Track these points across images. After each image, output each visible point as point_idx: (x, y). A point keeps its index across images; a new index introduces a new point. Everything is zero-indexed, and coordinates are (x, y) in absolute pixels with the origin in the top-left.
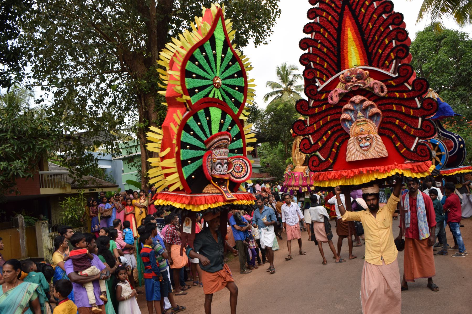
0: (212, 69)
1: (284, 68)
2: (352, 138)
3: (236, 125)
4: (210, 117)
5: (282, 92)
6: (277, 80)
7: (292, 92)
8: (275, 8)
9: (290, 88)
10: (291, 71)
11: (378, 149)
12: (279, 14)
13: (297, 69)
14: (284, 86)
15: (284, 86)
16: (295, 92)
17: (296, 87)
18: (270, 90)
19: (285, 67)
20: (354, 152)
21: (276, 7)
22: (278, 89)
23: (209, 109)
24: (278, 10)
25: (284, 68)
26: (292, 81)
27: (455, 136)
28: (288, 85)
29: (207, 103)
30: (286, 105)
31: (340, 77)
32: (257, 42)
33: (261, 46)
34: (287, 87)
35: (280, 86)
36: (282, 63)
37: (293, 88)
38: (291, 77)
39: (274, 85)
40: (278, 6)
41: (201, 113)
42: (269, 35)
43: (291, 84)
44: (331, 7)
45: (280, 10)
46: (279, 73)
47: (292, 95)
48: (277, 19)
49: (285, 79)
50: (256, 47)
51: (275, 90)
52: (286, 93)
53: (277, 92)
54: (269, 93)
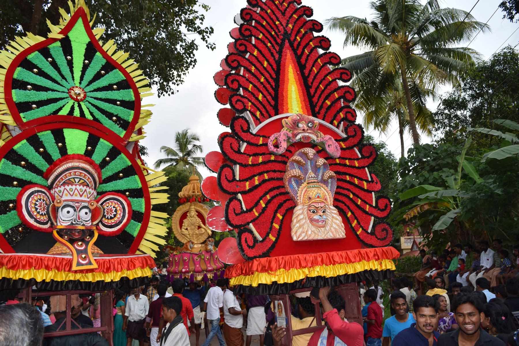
0: (93, 105)
1: (185, 135)
2: (299, 207)
3: (101, 140)
4: (64, 143)
5: (177, 161)
6: (174, 146)
7: (188, 163)
8: (190, 57)
9: (187, 158)
10: (192, 140)
11: (334, 228)
12: (193, 64)
13: (198, 139)
14: (181, 155)
15: (181, 155)
16: (191, 164)
17: (194, 158)
18: (163, 156)
19: (186, 134)
20: (302, 229)
21: (192, 55)
22: (173, 157)
23: (62, 133)
24: (193, 60)
25: (185, 135)
26: (190, 151)
27: (76, 249)
28: (185, 155)
29: (58, 125)
30: (180, 174)
31: (283, 120)
32: (163, 89)
33: (165, 97)
34: (184, 156)
35: (176, 154)
36: (183, 129)
37: (190, 160)
38: (190, 147)
39: (169, 151)
40: (194, 55)
41: (46, 137)
42: (178, 85)
43: (189, 154)
44: (267, 46)
45: (195, 61)
46: (177, 139)
47: (187, 166)
48: (190, 69)
49: (184, 148)
50: (159, 97)
51: (170, 157)
52: (181, 163)
53: (172, 160)
54: (163, 160)
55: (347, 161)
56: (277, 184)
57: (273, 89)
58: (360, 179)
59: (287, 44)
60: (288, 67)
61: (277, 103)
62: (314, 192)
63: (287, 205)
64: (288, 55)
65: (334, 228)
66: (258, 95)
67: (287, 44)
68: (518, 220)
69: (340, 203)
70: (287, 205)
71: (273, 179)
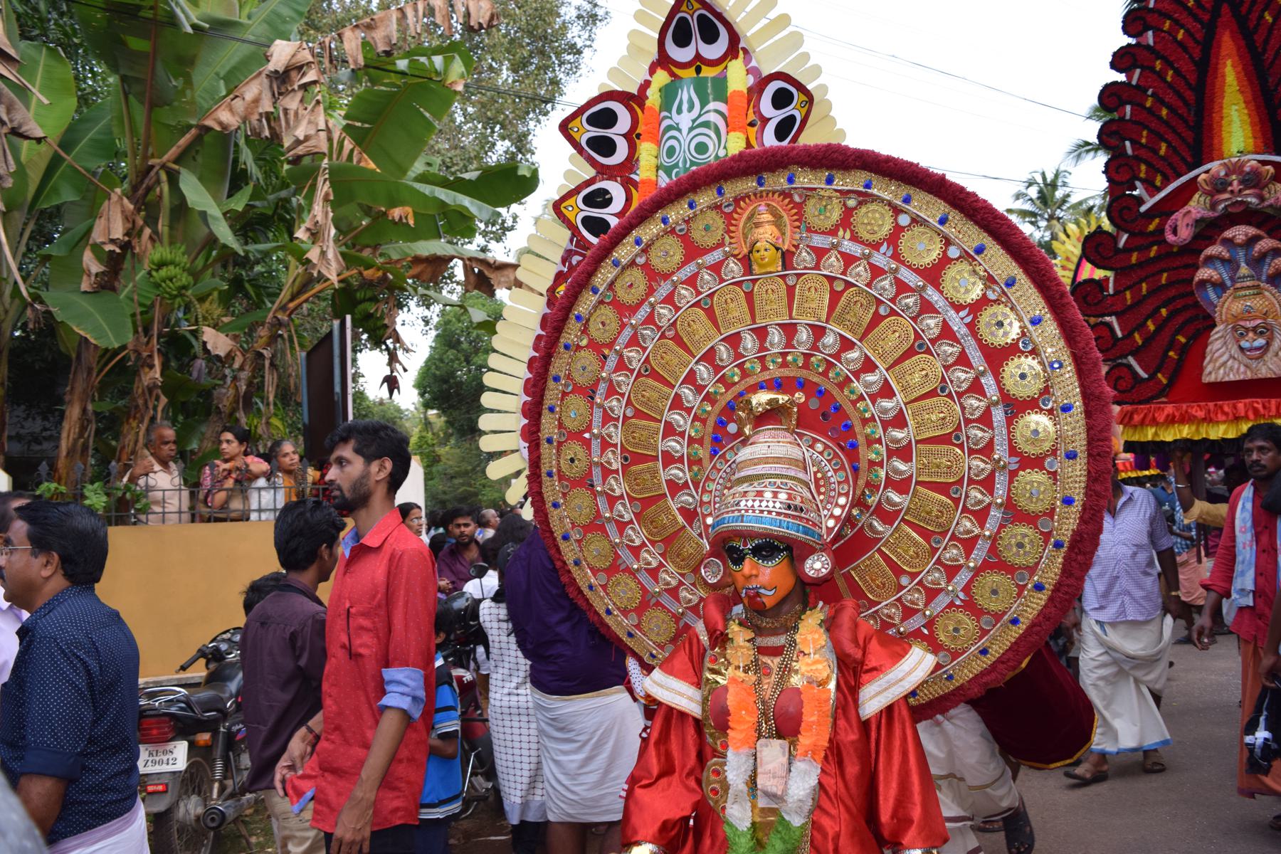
2: (1220, 327)
60: (1225, 66)
61: (1201, 143)
64: (1227, 43)
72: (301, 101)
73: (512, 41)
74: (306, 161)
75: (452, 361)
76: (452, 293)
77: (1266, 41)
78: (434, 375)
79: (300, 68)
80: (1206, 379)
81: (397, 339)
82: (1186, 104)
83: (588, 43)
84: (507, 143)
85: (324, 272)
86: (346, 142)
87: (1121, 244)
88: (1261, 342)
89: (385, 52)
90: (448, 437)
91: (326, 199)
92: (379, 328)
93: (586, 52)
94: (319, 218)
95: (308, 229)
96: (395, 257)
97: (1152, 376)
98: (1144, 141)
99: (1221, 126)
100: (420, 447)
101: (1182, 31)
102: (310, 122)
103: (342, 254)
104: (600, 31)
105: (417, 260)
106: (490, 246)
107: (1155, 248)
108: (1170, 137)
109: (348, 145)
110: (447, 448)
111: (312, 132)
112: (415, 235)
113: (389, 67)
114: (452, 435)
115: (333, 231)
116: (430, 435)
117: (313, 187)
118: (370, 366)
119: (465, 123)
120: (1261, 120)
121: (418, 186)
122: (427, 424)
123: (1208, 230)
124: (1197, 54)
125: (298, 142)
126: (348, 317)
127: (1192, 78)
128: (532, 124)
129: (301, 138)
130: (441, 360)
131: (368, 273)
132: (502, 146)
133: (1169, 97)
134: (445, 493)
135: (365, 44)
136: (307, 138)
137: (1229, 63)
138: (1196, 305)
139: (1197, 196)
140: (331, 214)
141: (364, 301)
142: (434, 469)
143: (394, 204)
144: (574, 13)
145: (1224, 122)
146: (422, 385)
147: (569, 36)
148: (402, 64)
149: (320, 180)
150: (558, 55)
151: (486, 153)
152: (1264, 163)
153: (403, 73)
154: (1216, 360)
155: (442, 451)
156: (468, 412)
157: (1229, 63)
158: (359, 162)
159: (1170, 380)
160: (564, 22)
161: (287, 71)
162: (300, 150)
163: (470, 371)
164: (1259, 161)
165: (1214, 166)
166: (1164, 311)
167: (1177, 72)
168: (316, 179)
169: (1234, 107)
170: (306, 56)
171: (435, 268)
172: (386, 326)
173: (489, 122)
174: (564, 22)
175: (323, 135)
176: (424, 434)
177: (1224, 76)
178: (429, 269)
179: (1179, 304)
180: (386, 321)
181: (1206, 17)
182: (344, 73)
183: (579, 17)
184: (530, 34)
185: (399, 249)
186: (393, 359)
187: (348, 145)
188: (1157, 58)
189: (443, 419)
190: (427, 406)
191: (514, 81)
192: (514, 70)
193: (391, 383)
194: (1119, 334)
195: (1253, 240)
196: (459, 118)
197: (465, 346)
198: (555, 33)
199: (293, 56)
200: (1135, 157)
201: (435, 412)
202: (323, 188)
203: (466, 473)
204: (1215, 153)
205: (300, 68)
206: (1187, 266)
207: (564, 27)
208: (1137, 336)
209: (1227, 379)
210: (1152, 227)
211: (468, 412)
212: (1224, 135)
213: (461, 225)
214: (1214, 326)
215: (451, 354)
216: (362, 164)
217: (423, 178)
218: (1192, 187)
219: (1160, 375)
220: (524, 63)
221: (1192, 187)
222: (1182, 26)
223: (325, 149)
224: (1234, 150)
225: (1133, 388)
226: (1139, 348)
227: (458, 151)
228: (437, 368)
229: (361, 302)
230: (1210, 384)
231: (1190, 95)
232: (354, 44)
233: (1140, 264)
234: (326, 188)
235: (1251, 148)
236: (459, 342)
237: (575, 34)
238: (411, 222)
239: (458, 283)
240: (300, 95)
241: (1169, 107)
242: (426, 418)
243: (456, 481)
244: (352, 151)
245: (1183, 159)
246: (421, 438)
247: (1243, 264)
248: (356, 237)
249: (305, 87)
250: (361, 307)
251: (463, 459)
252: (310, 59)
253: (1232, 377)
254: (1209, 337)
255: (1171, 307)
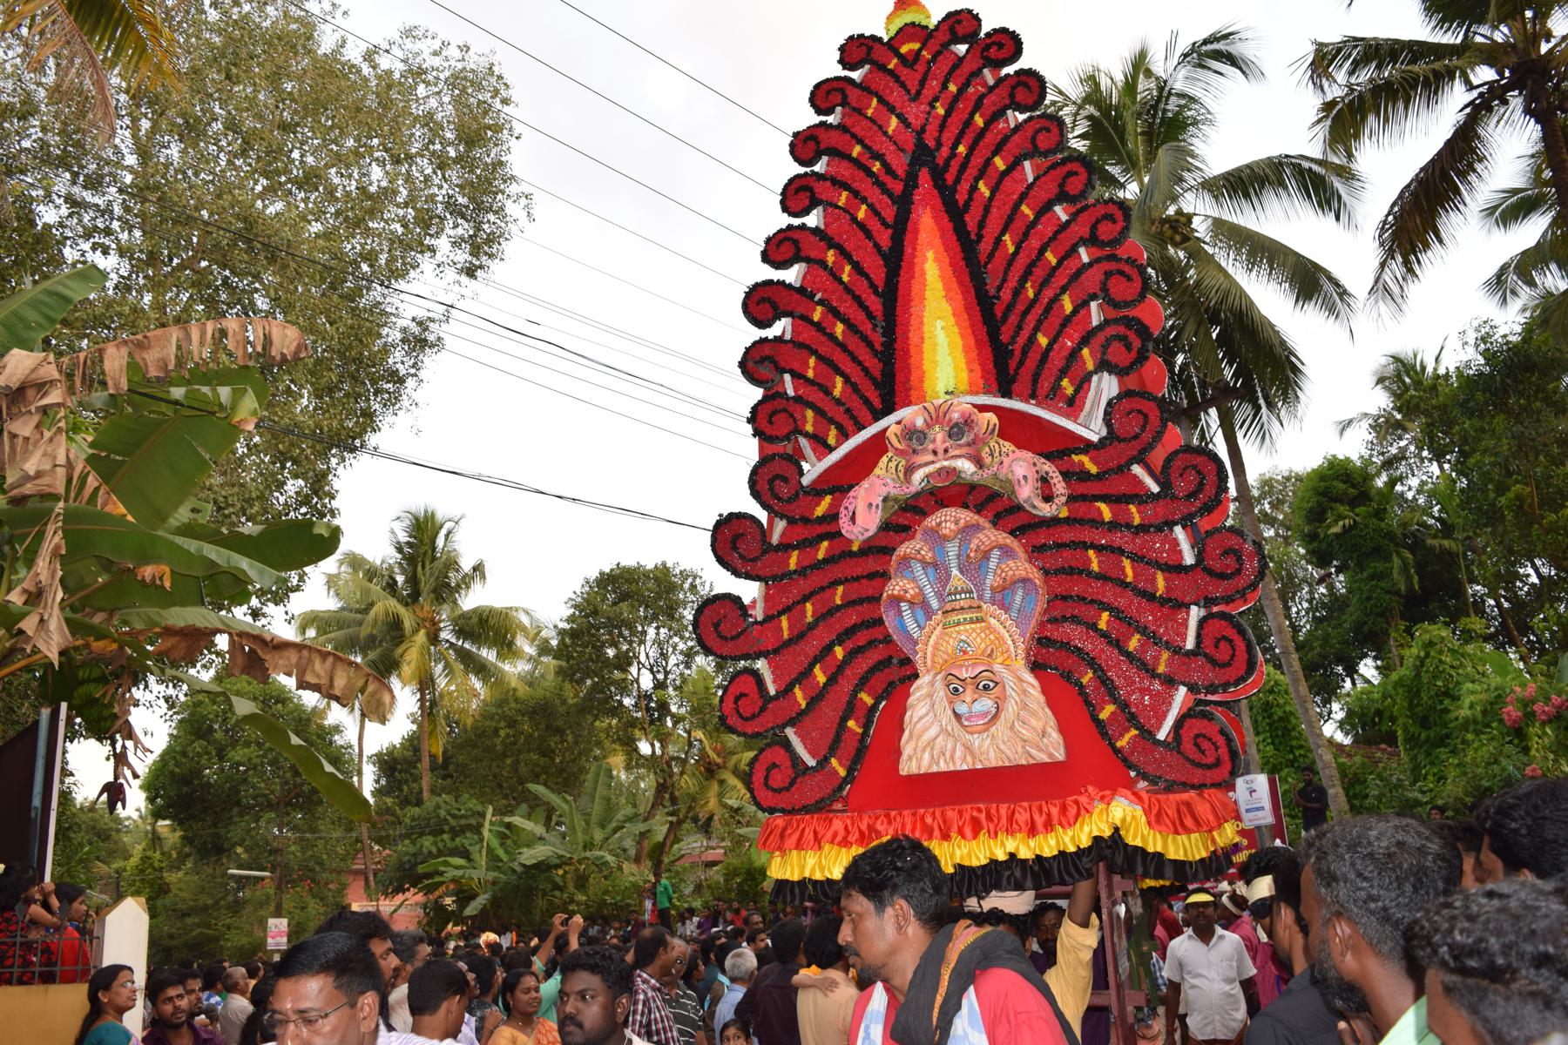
2: (924, 680)
11: (1026, 730)
55: (1104, 715)
56: (872, 657)
57: (877, 385)
58: (1115, 500)
59: (924, 176)
60: (925, 260)
61: (891, 381)
62: (969, 635)
63: (895, 673)
64: (927, 225)
65: (1026, 730)
66: (843, 392)
67: (924, 176)
68: (1530, 8)
69: (1049, 658)
70: (895, 673)
71: (859, 650)
72: (37, 427)
73: (319, 362)
74: (32, 505)
75: (199, 755)
76: (204, 674)
77: (981, 225)
78: (172, 773)
79: (42, 387)
80: (908, 767)
81: (129, 734)
82: (870, 315)
83: (413, 371)
84: (301, 482)
85: (42, 646)
86: (90, 478)
87: (775, 539)
88: (986, 704)
89: (158, 378)
90: (182, 858)
91: (55, 553)
92: (105, 719)
93: (410, 383)
94: (43, 578)
95: (25, 591)
96: (139, 626)
97: (823, 762)
98: (810, 374)
99: (921, 352)
100: (142, 871)
101: (864, 207)
102: (45, 454)
103: (68, 621)
104: (430, 360)
105: (169, 631)
106: (265, 610)
107: (825, 544)
108: (849, 367)
109: (92, 481)
110: (180, 874)
111: (48, 467)
112: (169, 599)
113: (160, 395)
114: (189, 855)
115: (60, 594)
116: (157, 855)
117: (40, 536)
118: (86, 765)
119: (248, 456)
120: (977, 341)
121: (180, 540)
122: (155, 839)
123: (906, 517)
124: (885, 238)
125: (27, 478)
126: (64, 705)
127: (879, 275)
128: (334, 461)
129: (32, 473)
130: (184, 754)
131: (98, 646)
132: (293, 486)
133: (847, 306)
134: (171, 936)
135: (133, 366)
136: (39, 475)
137: (930, 255)
138: (887, 640)
139: (885, 459)
140: (60, 573)
141: (88, 681)
142: (159, 903)
143: (146, 559)
144: (399, 335)
145: (926, 347)
146: (153, 787)
147: (391, 361)
148: (178, 393)
149: (51, 528)
150: (374, 382)
151: (271, 492)
152: (983, 408)
153: (176, 403)
154: (920, 736)
155: (172, 877)
156: (215, 825)
157: (930, 255)
158: (105, 504)
159: (850, 771)
160: (385, 344)
161: (22, 389)
162: (28, 489)
163: (222, 769)
164: (975, 406)
165: (908, 414)
166: (839, 652)
167: (858, 268)
168: (46, 524)
169: (939, 324)
170: (51, 372)
171: (196, 641)
172: (115, 717)
173: (281, 458)
174: (385, 344)
175: (61, 472)
176: (149, 853)
177: (923, 274)
178: (184, 644)
179: (862, 638)
180: (116, 710)
181: (897, 187)
182: (99, 397)
183: (403, 341)
184: (341, 355)
185: (137, 617)
186: (120, 759)
187: (92, 481)
188: (830, 248)
189: (179, 833)
190: (157, 814)
191: (315, 409)
192: (317, 394)
193: (114, 792)
194: (772, 692)
195: (969, 530)
196: (241, 450)
197: (219, 735)
198: (373, 355)
199: (33, 371)
200: (798, 399)
201: (167, 822)
202: (54, 538)
203: (205, 909)
204: (914, 394)
205: (42, 387)
206: (873, 576)
207: (386, 350)
208: (798, 693)
209: (935, 769)
210: (820, 511)
211: (215, 825)
212: (927, 366)
213: (234, 589)
214: (917, 676)
215: (198, 746)
216: (108, 509)
217: (188, 530)
218: (878, 445)
219: (834, 762)
220: (331, 390)
221: (878, 445)
222: (864, 200)
223: (61, 490)
224: (941, 387)
225: (792, 783)
226: (802, 713)
227: (236, 490)
228: (177, 764)
229: (83, 683)
230: (910, 777)
231: (875, 304)
232: (117, 365)
233: (801, 571)
234: (57, 539)
235: (964, 386)
236: (211, 730)
237: (398, 359)
238: (167, 584)
239: (218, 654)
240: (36, 419)
241: (846, 322)
242: (154, 831)
243: (189, 921)
244: (97, 489)
245: (867, 402)
246: (145, 859)
247: (955, 572)
248: (87, 597)
249: (44, 410)
250: (82, 690)
251: (202, 890)
252: (56, 375)
253: (943, 767)
254: (908, 695)
255: (850, 645)
